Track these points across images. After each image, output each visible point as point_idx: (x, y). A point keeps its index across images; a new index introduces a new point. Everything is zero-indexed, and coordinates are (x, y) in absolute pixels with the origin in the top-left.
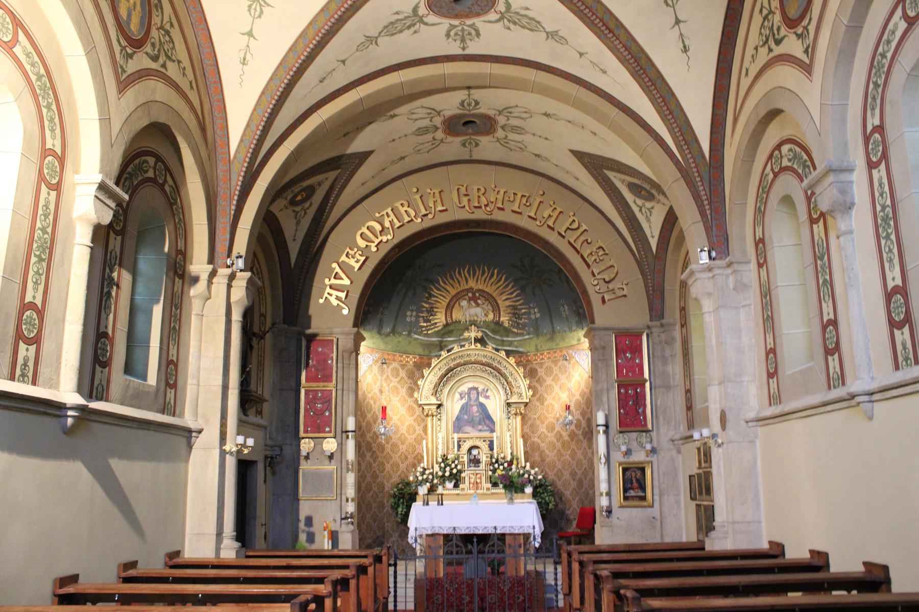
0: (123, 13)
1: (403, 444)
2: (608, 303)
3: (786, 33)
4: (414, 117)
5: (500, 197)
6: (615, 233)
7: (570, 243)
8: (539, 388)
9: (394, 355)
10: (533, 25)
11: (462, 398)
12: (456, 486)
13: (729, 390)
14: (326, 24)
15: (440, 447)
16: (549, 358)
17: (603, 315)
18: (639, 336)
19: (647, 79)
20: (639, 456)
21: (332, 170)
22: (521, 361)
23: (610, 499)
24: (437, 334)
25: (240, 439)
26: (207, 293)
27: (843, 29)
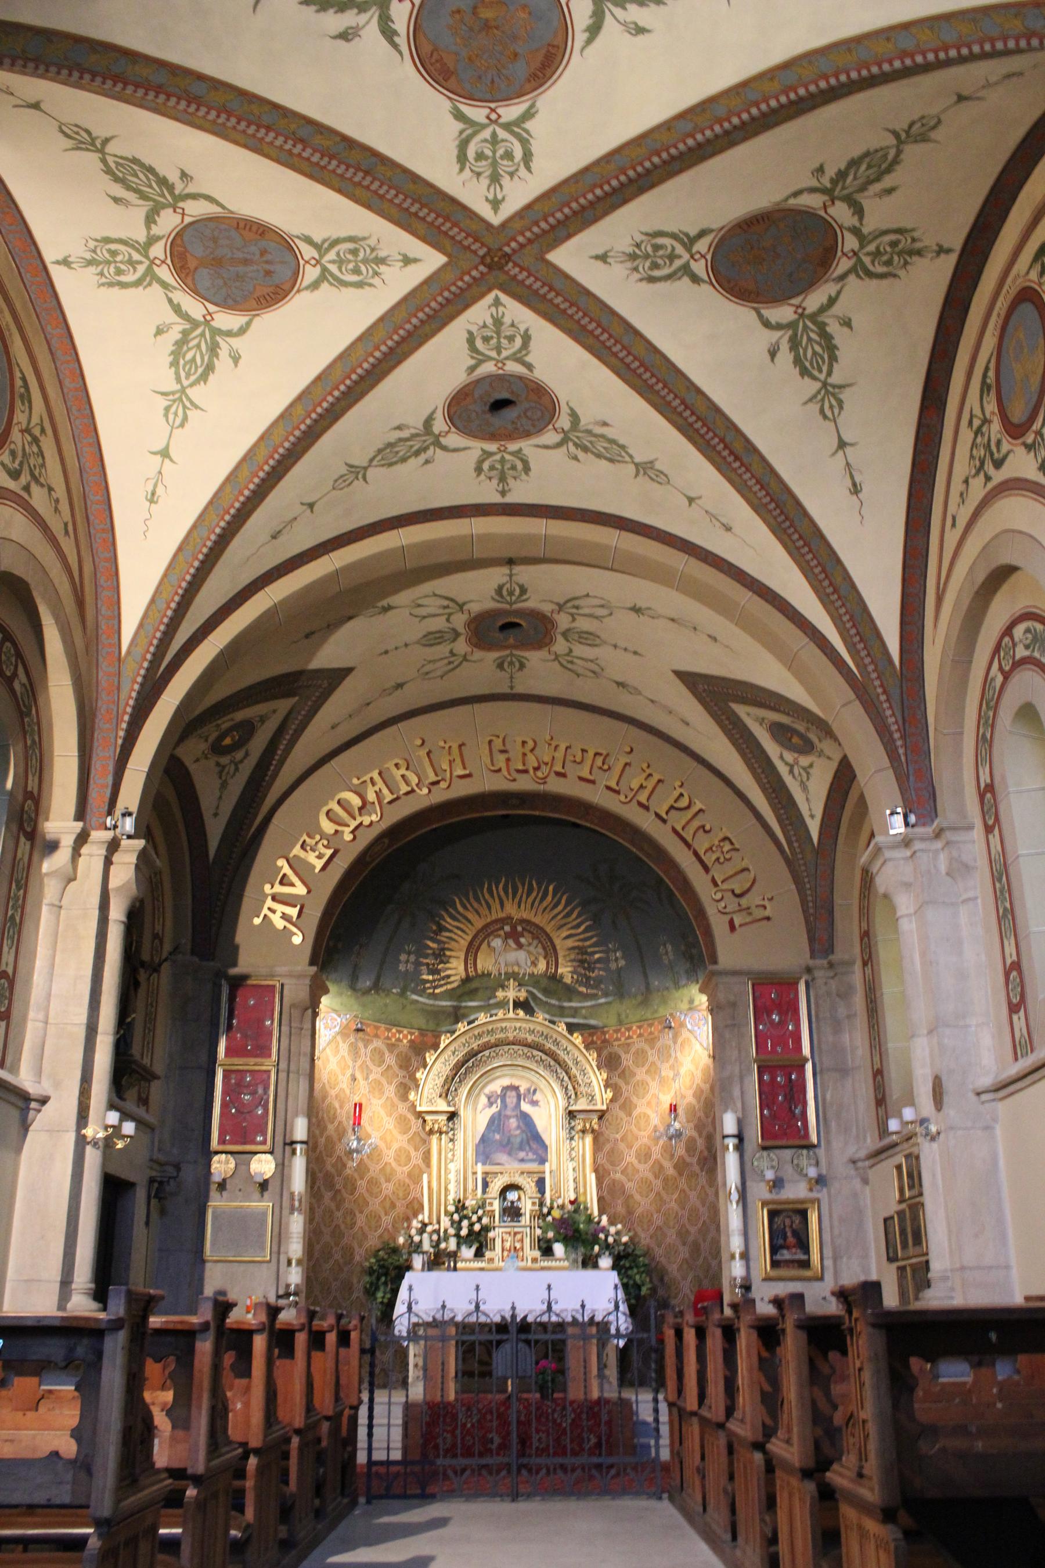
1: (388, 1180)
2: (739, 930)
3: (1010, 447)
4: (423, 611)
5: (560, 755)
6: (750, 815)
8: (624, 1087)
9: (377, 1028)
10: (613, 451)
11: (491, 1104)
12: (479, 1254)
14: (287, 439)
15: (452, 1187)
16: (640, 1036)
17: (731, 950)
18: (792, 985)
19: (796, 536)
20: (796, 1191)
22: (593, 1042)
23: (748, 1268)
24: (450, 994)
25: (113, 1117)
26: (71, 870)
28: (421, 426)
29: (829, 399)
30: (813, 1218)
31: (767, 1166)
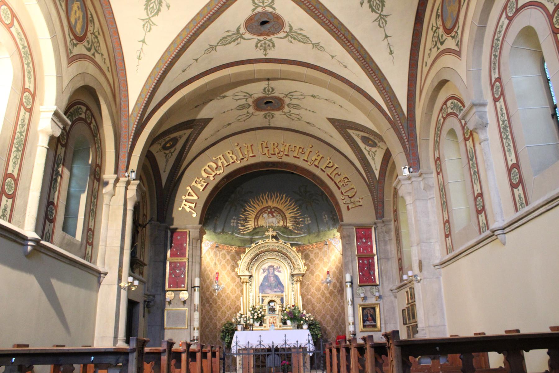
0: (73, 21)
1: (228, 300)
2: (351, 210)
4: (237, 98)
5: (287, 148)
6: (354, 169)
7: (328, 175)
10: (305, 40)
11: (264, 272)
12: (261, 325)
13: (423, 248)
15: (251, 301)
16: (316, 247)
17: (348, 217)
20: (371, 301)
21: (187, 129)
24: (249, 234)
25: (130, 279)
26: (113, 192)
27: (475, 28)
28: (235, 30)
29: (382, 20)
30: (377, 310)
31: (361, 292)
